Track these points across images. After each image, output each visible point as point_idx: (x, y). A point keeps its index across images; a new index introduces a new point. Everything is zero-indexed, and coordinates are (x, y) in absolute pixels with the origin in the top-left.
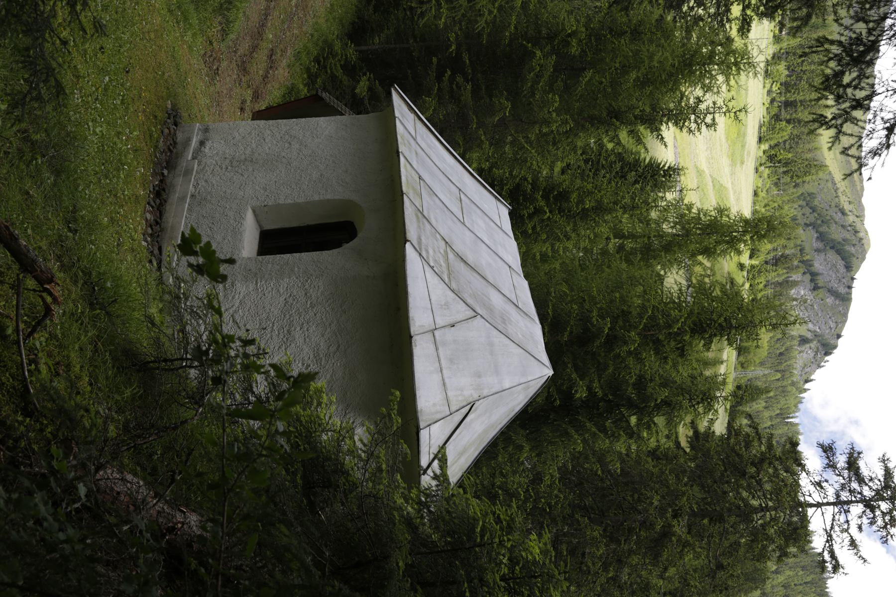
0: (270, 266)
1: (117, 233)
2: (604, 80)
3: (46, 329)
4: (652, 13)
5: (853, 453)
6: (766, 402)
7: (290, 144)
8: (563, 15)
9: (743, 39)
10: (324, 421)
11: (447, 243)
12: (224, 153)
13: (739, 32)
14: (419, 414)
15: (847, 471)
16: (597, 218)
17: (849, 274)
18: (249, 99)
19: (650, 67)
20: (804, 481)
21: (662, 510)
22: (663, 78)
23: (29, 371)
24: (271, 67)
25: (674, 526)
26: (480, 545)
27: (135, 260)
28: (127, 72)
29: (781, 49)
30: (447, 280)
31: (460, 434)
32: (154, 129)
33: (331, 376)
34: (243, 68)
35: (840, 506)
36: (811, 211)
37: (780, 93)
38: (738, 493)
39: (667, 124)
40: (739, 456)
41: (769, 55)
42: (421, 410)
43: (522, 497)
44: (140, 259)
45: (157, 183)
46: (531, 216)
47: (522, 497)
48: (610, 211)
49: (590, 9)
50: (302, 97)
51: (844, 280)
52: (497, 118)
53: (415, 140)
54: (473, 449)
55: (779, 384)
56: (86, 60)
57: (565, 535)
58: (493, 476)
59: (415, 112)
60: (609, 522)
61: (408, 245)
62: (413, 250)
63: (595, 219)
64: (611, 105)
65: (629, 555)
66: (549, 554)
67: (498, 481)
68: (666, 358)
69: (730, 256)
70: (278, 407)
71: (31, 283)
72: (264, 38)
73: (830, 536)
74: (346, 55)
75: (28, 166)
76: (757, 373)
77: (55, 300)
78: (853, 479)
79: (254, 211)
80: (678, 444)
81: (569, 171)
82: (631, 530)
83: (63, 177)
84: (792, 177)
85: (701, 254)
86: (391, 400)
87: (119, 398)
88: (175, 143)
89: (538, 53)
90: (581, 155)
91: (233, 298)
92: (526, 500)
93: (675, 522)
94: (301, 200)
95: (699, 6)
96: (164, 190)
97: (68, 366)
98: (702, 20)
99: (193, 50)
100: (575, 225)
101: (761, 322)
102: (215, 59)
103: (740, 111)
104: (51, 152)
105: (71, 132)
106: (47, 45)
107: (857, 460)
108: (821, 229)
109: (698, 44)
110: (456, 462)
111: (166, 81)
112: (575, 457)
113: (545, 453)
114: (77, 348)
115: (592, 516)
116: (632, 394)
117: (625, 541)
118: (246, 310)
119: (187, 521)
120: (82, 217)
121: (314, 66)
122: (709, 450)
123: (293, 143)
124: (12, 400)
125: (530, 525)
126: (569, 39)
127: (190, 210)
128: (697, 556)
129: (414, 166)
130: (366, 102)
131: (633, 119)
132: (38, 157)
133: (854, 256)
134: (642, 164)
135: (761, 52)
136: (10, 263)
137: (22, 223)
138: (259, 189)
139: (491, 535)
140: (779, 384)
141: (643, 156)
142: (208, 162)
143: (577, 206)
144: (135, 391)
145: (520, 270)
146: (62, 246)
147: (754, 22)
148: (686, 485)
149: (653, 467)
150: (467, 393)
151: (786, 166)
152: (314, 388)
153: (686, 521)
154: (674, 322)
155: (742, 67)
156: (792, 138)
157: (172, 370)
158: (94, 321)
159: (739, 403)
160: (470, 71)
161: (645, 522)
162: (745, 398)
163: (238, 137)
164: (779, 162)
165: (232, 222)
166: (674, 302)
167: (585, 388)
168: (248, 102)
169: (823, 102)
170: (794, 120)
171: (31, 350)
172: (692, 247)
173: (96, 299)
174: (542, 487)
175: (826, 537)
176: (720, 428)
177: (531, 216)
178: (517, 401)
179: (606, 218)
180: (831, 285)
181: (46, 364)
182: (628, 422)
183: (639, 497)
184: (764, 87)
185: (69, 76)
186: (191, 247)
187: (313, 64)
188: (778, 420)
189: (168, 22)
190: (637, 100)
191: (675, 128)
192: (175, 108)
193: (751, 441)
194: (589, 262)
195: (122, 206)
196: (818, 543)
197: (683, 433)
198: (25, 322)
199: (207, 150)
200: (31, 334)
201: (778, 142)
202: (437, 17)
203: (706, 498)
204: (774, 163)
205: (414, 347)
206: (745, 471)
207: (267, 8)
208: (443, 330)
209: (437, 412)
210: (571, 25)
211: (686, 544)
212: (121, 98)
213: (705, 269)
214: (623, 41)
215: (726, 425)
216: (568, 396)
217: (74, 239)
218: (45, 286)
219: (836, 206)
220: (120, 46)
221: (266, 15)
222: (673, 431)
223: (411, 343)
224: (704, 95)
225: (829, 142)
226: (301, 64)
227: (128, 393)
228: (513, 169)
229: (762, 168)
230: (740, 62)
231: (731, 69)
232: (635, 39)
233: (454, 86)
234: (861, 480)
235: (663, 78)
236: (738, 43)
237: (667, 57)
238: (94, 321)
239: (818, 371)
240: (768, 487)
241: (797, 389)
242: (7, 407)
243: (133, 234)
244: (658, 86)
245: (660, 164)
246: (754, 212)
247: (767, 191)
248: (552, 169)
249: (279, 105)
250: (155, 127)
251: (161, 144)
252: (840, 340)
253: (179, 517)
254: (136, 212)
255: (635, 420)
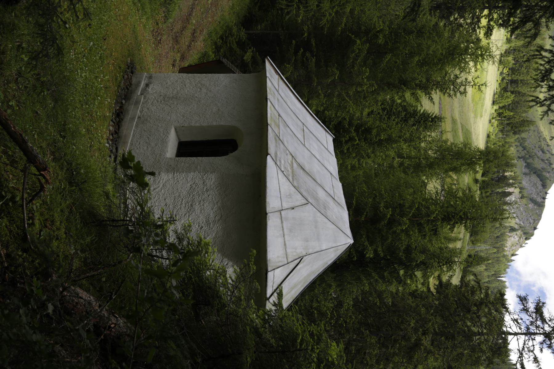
0: (183, 164)
1: (90, 138)
2: (398, 61)
3: (40, 198)
4: (431, 20)
5: (539, 303)
6: (486, 266)
7: (201, 89)
8: (375, 19)
9: (487, 39)
10: (208, 264)
11: (293, 157)
12: (160, 92)
13: (485, 35)
14: (268, 262)
15: (534, 314)
16: (388, 146)
17: (544, 190)
18: (178, 59)
19: (427, 54)
20: (507, 318)
21: (416, 330)
22: (435, 61)
23: (28, 224)
24: (193, 40)
25: (423, 340)
26: (299, 350)
27: (100, 155)
28: (105, 40)
29: (511, 47)
30: (291, 180)
31: (293, 276)
32: (118, 75)
33: (216, 235)
34: (176, 40)
35: (529, 336)
36: (522, 149)
37: (508, 75)
38: (465, 322)
39: (436, 90)
40: (468, 300)
41: (503, 50)
42: (270, 260)
43: (329, 316)
44: (103, 155)
45: (118, 108)
46: (347, 142)
47: (329, 316)
48: (396, 142)
49: (392, 16)
50: (211, 60)
51: (541, 194)
52: (330, 80)
53: (278, 91)
54: (300, 286)
55: (495, 255)
56: (79, 32)
57: (354, 340)
58: (312, 301)
59: (279, 75)
60: (382, 335)
61: (269, 157)
62: (272, 160)
63: (386, 146)
64: (401, 76)
65: (393, 356)
66: (342, 358)
67: (315, 305)
68: (425, 235)
69: (470, 173)
70: (174, 270)
71: (33, 169)
72: (190, 22)
73: (521, 354)
74: (240, 36)
75: (38, 96)
76: (482, 248)
77: (47, 181)
78: (538, 319)
79: (176, 129)
80: (429, 289)
81: (373, 116)
82: (395, 341)
83: (60, 103)
84: (512, 127)
85: (451, 171)
86: (251, 255)
87: (83, 242)
88: (131, 84)
89: (358, 42)
90: (381, 105)
91: (159, 182)
92: (332, 318)
93: (423, 338)
94: (205, 124)
95: (461, 18)
96: (122, 113)
97: (53, 222)
98: (462, 26)
99: (146, 28)
100: (374, 149)
101: (487, 216)
102: (159, 34)
103: (482, 85)
104: (53, 88)
105: (67, 76)
106: (53, 24)
107: (542, 308)
108: (528, 161)
109: (458, 42)
110: (289, 293)
111: (128, 46)
112: (363, 293)
113: (345, 289)
114: (59, 210)
115: (372, 330)
116: (403, 256)
117: (391, 347)
118: (166, 190)
119: (118, 323)
120: (69, 129)
121: (220, 41)
122: (447, 295)
123: (202, 89)
124: (16, 241)
125: (333, 333)
126: (378, 34)
127: (137, 126)
128: (436, 360)
129: (276, 108)
130: (250, 65)
131: (415, 86)
132: (45, 90)
133: (548, 179)
134: (418, 114)
135: (498, 48)
136: (22, 156)
137: (32, 131)
138: (180, 116)
139: (307, 344)
140: (495, 255)
141: (419, 108)
142: (150, 97)
143: (376, 138)
144: (93, 238)
145: (338, 177)
146: (55, 146)
147: (495, 29)
148: (432, 315)
149: (412, 302)
150: (299, 251)
151: (509, 120)
152: (204, 242)
153: (430, 338)
154: (431, 213)
155: (485, 57)
156: (514, 102)
157: (117, 226)
158: (71, 193)
159: (468, 266)
160: (315, 50)
161: (405, 336)
162: (473, 263)
163: (169, 83)
164: (505, 117)
165: (162, 135)
166: (432, 199)
167: (372, 252)
168: (178, 61)
169: (539, 89)
170: (516, 92)
171: (31, 211)
172: (446, 167)
173: (74, 180)
174: (342, 311)
175: (519, 354)
176: (456, 281)
177: (347, 142)
178: (330, 258)
179: (393, 146)
180: (532, 196)
181: (39, 219)
182: (398, 273)
183: (402, 321)
184: (498, 70)
185: (68, 41)
186: (128, 164)
187: (219, 40)
188: (493, 278)
189: (132, 10)
190: (418, 74)
191: (440, 93)
192: (132, 63)
193: (475, 291)
194: (381, 171)
195: (95, 122)
196: (514, 357)
197: (433, 282)
198: (28, 193)
199: (150, 90)
200: (31, 201)
201: (505, 105)
202: (297, 15)
203: (444, 324)
204: (501, 118)
205: (268, 221)
206: (470, 309)
207: (193, 4)
208: (287, 210)
209: (279, 262)
210: (380, 25)
211: (429, 352)
212: (99, 55)
213: (453, 180)
214: (411, 37)
215: (460, 280)
216: (362, 255)
217: (63, 142)
218: (41, 173)
219: (539, 147)
220: (102, 24)
221: (192, 9)
222: (427, 281)
223: (266, 218)
224: (460, 74)
225: (541, 115)
226: (212, 40)
227: (88, 239)
228: (338, 112)
229: (494, 120)
230: (484, 54)
231: (479, 58)
232: (419, 36)
233: (305, 59)
234: (544, 320)
235: (435, 61)
236: (484, 42)
237: (438, 49)
238: (71, 193)
239: (520, 249)
240: (484, 320)
241: (506, 259)
242: (13, 246)
243: (100, 139)
244: (431, 66)
245: (430, 114)
246: (487, 148)
247: (496, 135)
248: (362, 114)
249: (196, 65)
250: (119, 74)
251: (122, 85)
252: (536, 231)
253: (114, 320)
254: (103, 126)
255: (403, 273)
